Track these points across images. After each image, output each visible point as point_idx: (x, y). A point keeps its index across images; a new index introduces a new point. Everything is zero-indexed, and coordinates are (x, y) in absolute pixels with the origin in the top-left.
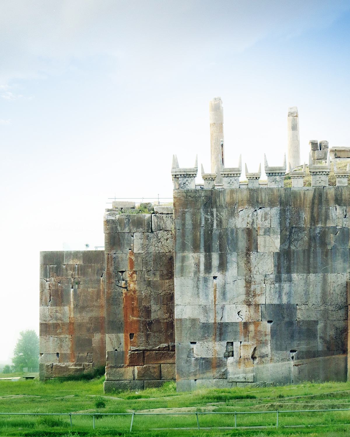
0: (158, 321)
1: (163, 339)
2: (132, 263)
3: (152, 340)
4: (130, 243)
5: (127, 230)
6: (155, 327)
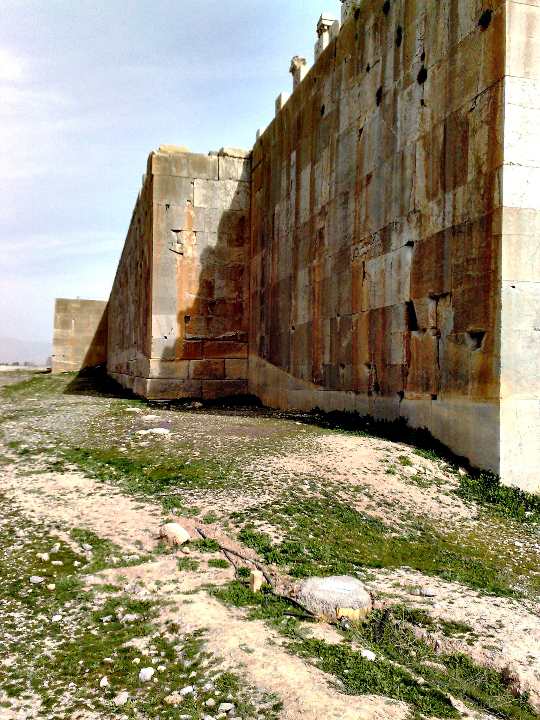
0: (222, 301)
1: (229, 326)
2: (190, 219)
3: (215, 325)
4: (189, 191)
5: (185, 173)
6: (219, 310)
